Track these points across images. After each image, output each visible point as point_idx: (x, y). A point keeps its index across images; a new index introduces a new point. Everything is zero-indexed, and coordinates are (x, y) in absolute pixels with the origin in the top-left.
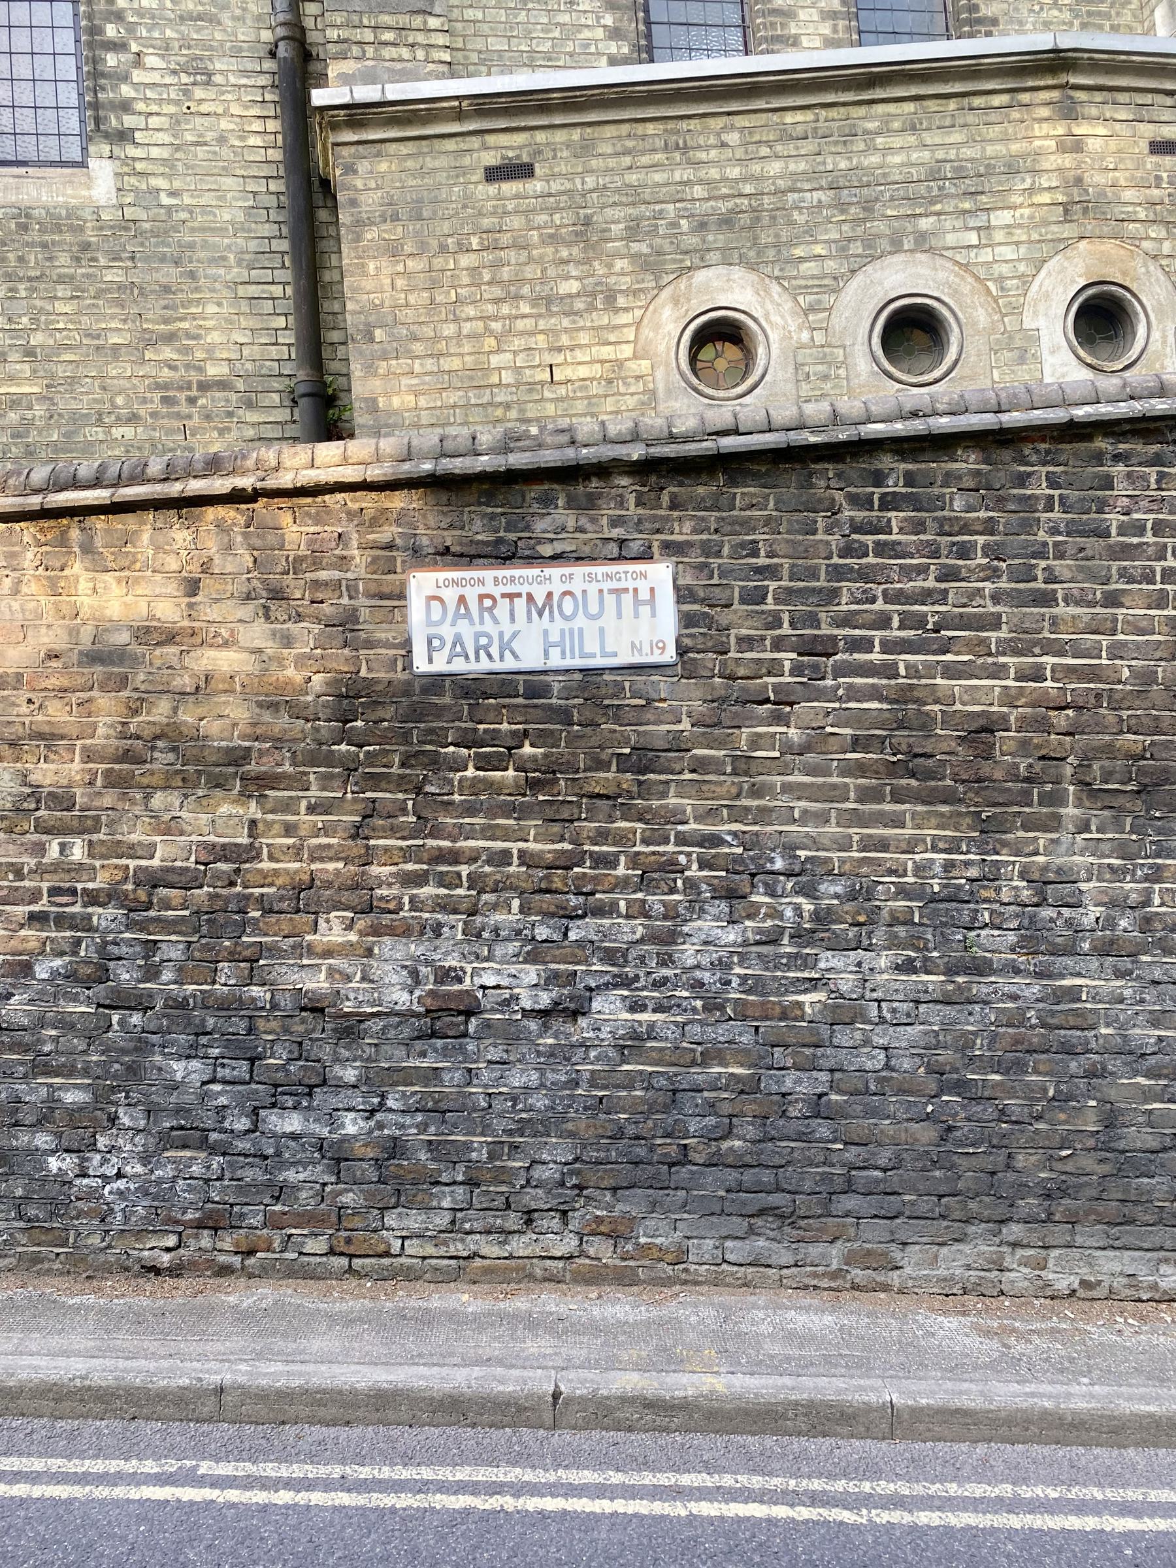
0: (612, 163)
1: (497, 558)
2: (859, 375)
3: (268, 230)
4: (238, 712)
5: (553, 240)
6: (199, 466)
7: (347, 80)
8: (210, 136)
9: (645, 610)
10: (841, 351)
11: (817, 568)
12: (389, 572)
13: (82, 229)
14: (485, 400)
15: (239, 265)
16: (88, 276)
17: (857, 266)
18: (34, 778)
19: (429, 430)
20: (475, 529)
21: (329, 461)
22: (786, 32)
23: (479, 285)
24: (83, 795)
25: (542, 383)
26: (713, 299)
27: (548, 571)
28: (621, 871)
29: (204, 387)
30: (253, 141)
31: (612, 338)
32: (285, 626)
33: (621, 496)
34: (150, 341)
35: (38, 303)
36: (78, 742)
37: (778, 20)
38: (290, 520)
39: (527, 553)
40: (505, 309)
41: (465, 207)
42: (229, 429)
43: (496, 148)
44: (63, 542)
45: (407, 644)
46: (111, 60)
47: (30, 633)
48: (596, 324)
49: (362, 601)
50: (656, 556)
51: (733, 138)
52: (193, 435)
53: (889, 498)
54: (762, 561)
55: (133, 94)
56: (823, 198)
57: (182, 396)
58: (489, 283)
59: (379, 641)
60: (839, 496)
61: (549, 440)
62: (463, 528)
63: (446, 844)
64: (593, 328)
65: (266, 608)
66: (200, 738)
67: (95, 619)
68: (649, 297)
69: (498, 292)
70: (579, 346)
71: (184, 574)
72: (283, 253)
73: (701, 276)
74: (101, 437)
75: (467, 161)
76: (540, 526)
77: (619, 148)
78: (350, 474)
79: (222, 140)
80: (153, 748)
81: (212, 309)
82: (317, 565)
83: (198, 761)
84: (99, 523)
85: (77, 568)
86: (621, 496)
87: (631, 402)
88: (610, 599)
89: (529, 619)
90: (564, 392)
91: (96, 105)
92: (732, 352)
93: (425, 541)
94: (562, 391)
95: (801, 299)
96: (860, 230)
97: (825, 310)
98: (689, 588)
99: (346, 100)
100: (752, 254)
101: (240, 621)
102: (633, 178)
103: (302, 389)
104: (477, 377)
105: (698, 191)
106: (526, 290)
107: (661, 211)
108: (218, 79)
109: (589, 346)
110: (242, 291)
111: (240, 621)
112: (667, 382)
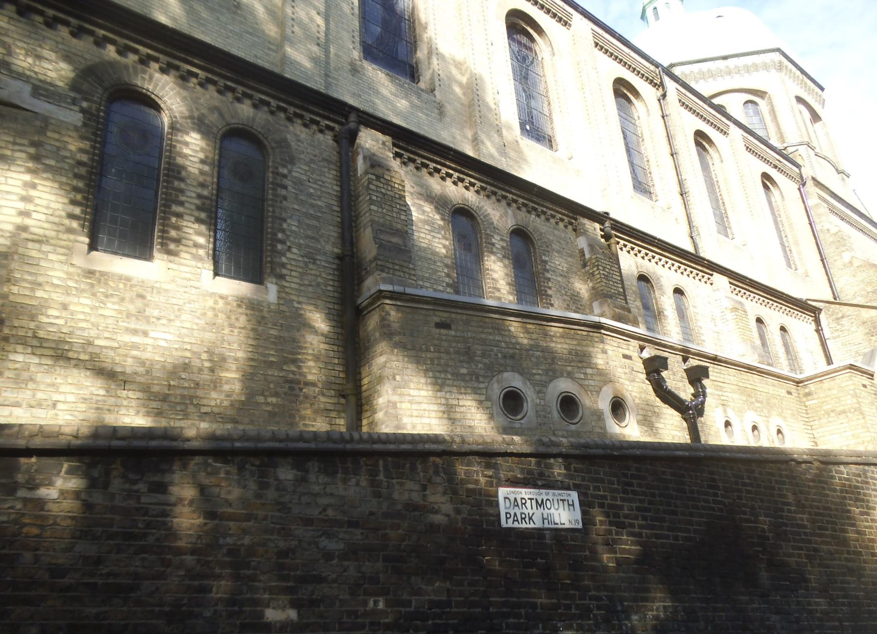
9: (571, 508)
18: (364, 569)
28: (573, 611)
30: (329, 288)
36: (382, 553)
45: (499, 515)
63: (515, 599)
74: (263, 401)
75: (429, 319)
88: (561, 503)
102: (483, 336)
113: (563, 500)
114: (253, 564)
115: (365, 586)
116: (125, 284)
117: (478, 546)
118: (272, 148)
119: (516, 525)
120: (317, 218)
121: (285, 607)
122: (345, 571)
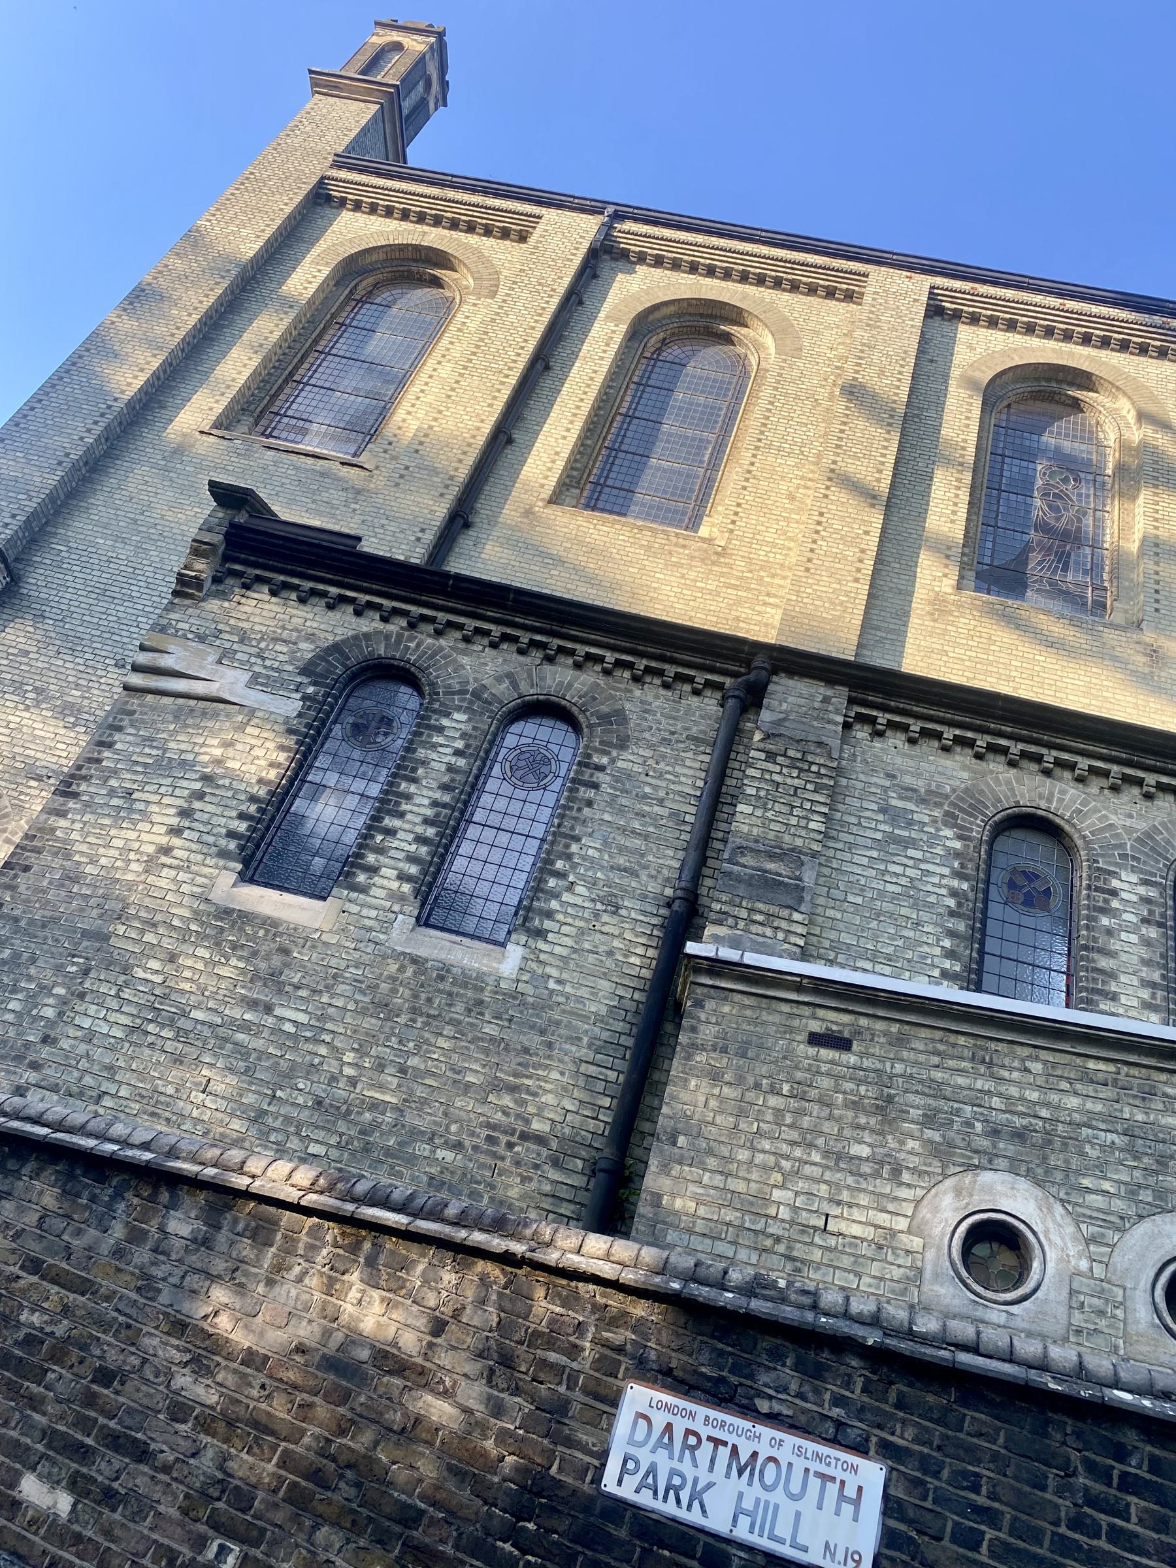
0: (922, 1058)
1: (714, 1396)
2: (1137, 1322)
3: (620, 1026)
4: (428, 1468)
5: (856, 1106)
6: (487, 1221)
7: (717, 939)
8: (602, 949)
9: (848, 1509)
10: (1121, 1292)
11: (1042, 1531)
12: (610, 1375)
13: (482, 989)
14: (758, 1227)
15: (589, 1047)
16: (471, 1025)
17: (1145, 1213)
18: (232, 1465)
19: (700, 1238)
20: (701, 1359)
21: (595, 1252)
22: (1106, 988)
23: (780, 1125)
24: (263, 1500)
25: (815, 1228)
26: (994, 1201)
27: (760, 1429)
29: (524, 1136)
30: (636, 960)
31: (890, 1207)
32: (502, 1395)
33: (849, 1376)
34: (497, 1086)
35: (427, 1035)
36: (283, 1444)
37: (1101, 977)
38: (542, 1294)
39: (745, 1401)
40: (798, 1152)
41: (785, 1058)
42: (530, 1179)
43: (823, 1020)
44: (354, 1249)
45: (603, 1456)
46: (552, 882)
47: (292, 1322)
48: (878, 1190)
49: (578, 1395)
50: (872, 1453)
51: (1037, 1067)
52: (500, 1175)
53: (1130, 1479)
54: (981, 1500)
55: (558, 908)
56: (1117, 1141)
57: (504, 1139)
58: (789, 1126)
59: (579, 1442)
60: (1075, 1456)
61: (793, 1297)
62: (690, 1355)
64: (874, 1193)
65: (492, 1371)
66: (386, 1482)
67: (349, 1328)
68: (933, 1182)
69: (794, 1135)
70: (858, 1205)
71: (437, 1313)
72: (627, 1048)
73: (986, 1177)
74: (426, 1154)
75: (796, 1023)
76: (764, 1378)
77: (930, 1047)
78: (607, 1270)
79: (610, 953)
80: (341, 1476)
81: (555, 1075)
82: (551, 1345)
83: (374, 1506)
84: (390, 1243)
85: (354, 1277)
86: (849, 1376)
87: (897, 1273)
88: (814, 1483)
89: (728, 1475)
90: (833, 1243)
91: (529, 909)
92: (1006, 1258)
93: (653, 1356)
94: (832, 1241)
95: (1083, 1227)
96: (1151, 1181)
97: (1107, 1245)
98: (899, 1501)
99: (712, 954)
100: (1040, 1171)
101: (465, 1375)
102: (938, 1075)
103: (603, 1165)
104: (756, 1205)
105: (996, 1102)
106: (820, 1141)
107: (958, 1110)
108: (623, 912)
109: (867, 1208)
110: (584, 1068)
111: (465, 1375)
112: (936, 1265)
113: (825, 1478)
114: (51, 1376)
115: (220, 1505)
116: (267, 931)
117: (519, 1519)
118: (590, 726)
119: (644, 1499)
120: (646, 837)
121: (58, 1482)
122: (193, 1455)
